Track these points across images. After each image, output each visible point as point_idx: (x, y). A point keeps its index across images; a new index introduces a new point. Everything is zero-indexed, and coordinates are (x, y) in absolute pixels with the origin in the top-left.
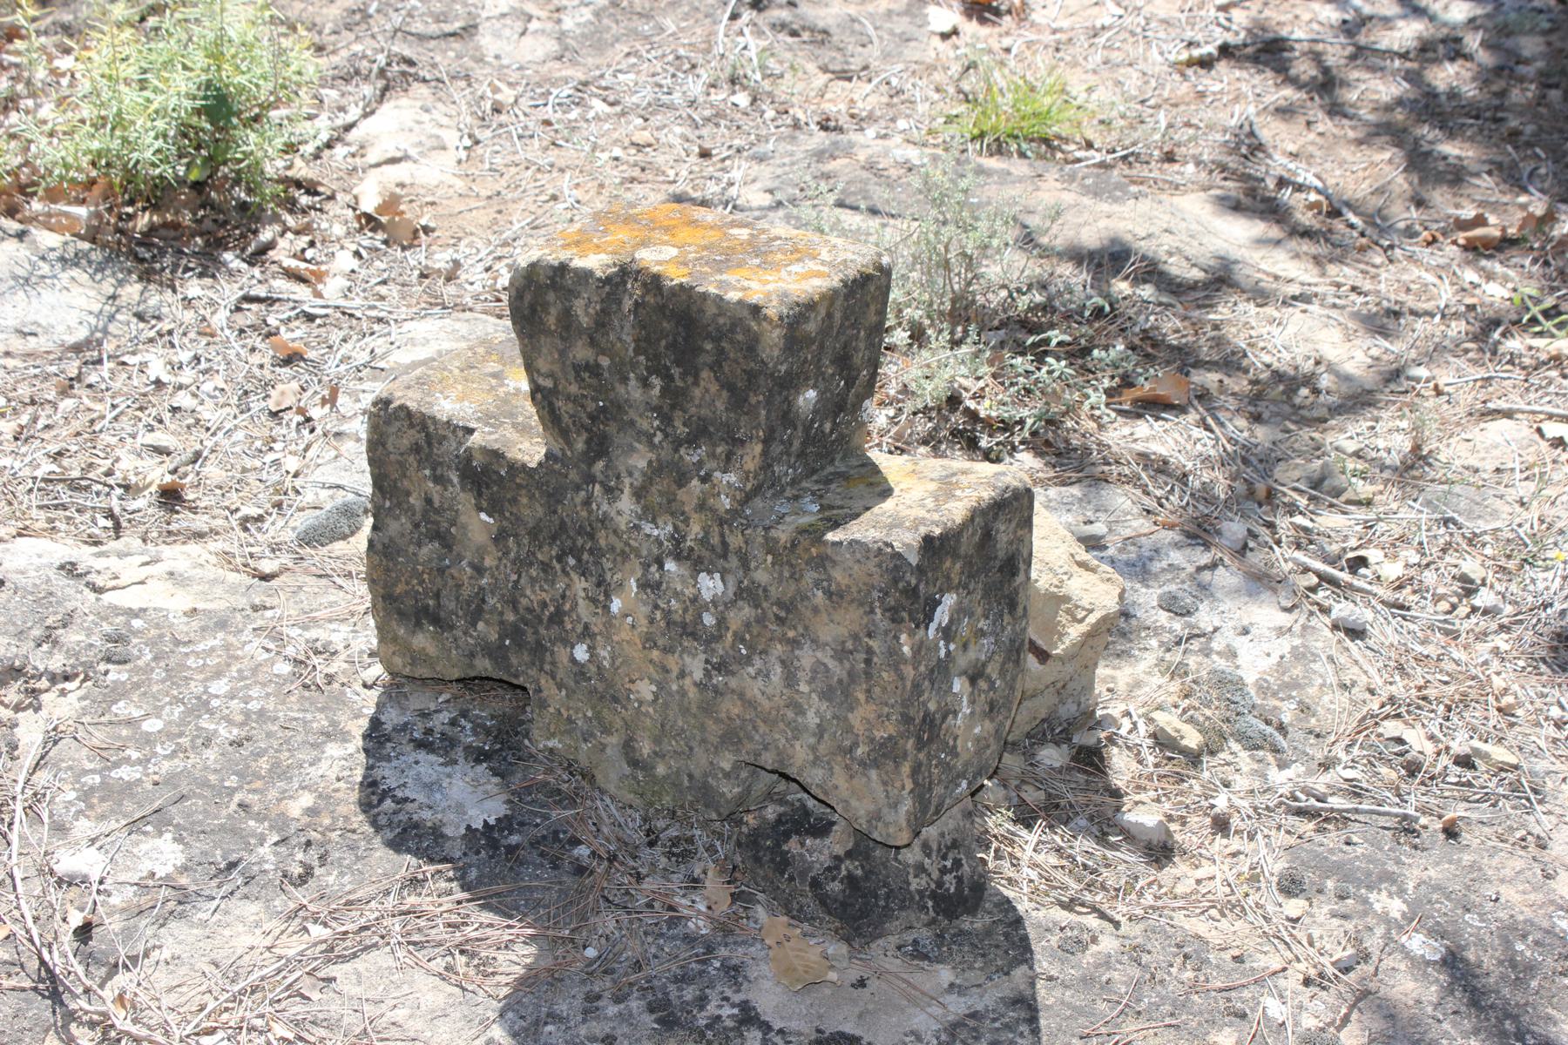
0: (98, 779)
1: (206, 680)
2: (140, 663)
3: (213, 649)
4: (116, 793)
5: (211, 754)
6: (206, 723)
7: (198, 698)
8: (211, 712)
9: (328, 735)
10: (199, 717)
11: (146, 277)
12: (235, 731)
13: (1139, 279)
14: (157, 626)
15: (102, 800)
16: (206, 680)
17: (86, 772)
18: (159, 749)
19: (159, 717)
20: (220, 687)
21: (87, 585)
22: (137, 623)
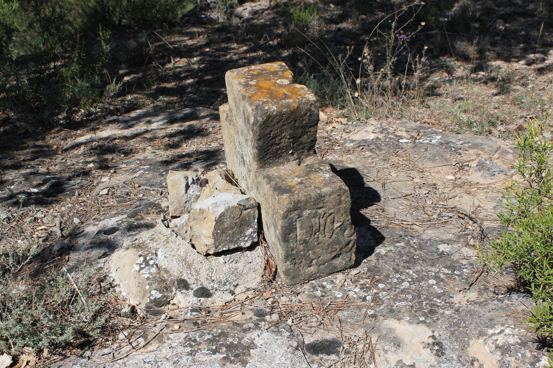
0: (455, 272)
1: (409, 289)
2: (428, 302)
3: (400, 301)
4: (452, 268)
5: (418, 268)
6: (415, 276)
7: (414, 283)
8: (412, 278)
9: (382, 257)
10: (417, 278)
11: (352, 224)
12: (407, 271)
13: (245, 63)
14: (415, 316)
15: (456, 267)
16: (409, 289)
17: (459, 276)
18: (433, 274)
19: (429, 284)
20: (406, 284)
21: (436, 339)
22: (422, 319)
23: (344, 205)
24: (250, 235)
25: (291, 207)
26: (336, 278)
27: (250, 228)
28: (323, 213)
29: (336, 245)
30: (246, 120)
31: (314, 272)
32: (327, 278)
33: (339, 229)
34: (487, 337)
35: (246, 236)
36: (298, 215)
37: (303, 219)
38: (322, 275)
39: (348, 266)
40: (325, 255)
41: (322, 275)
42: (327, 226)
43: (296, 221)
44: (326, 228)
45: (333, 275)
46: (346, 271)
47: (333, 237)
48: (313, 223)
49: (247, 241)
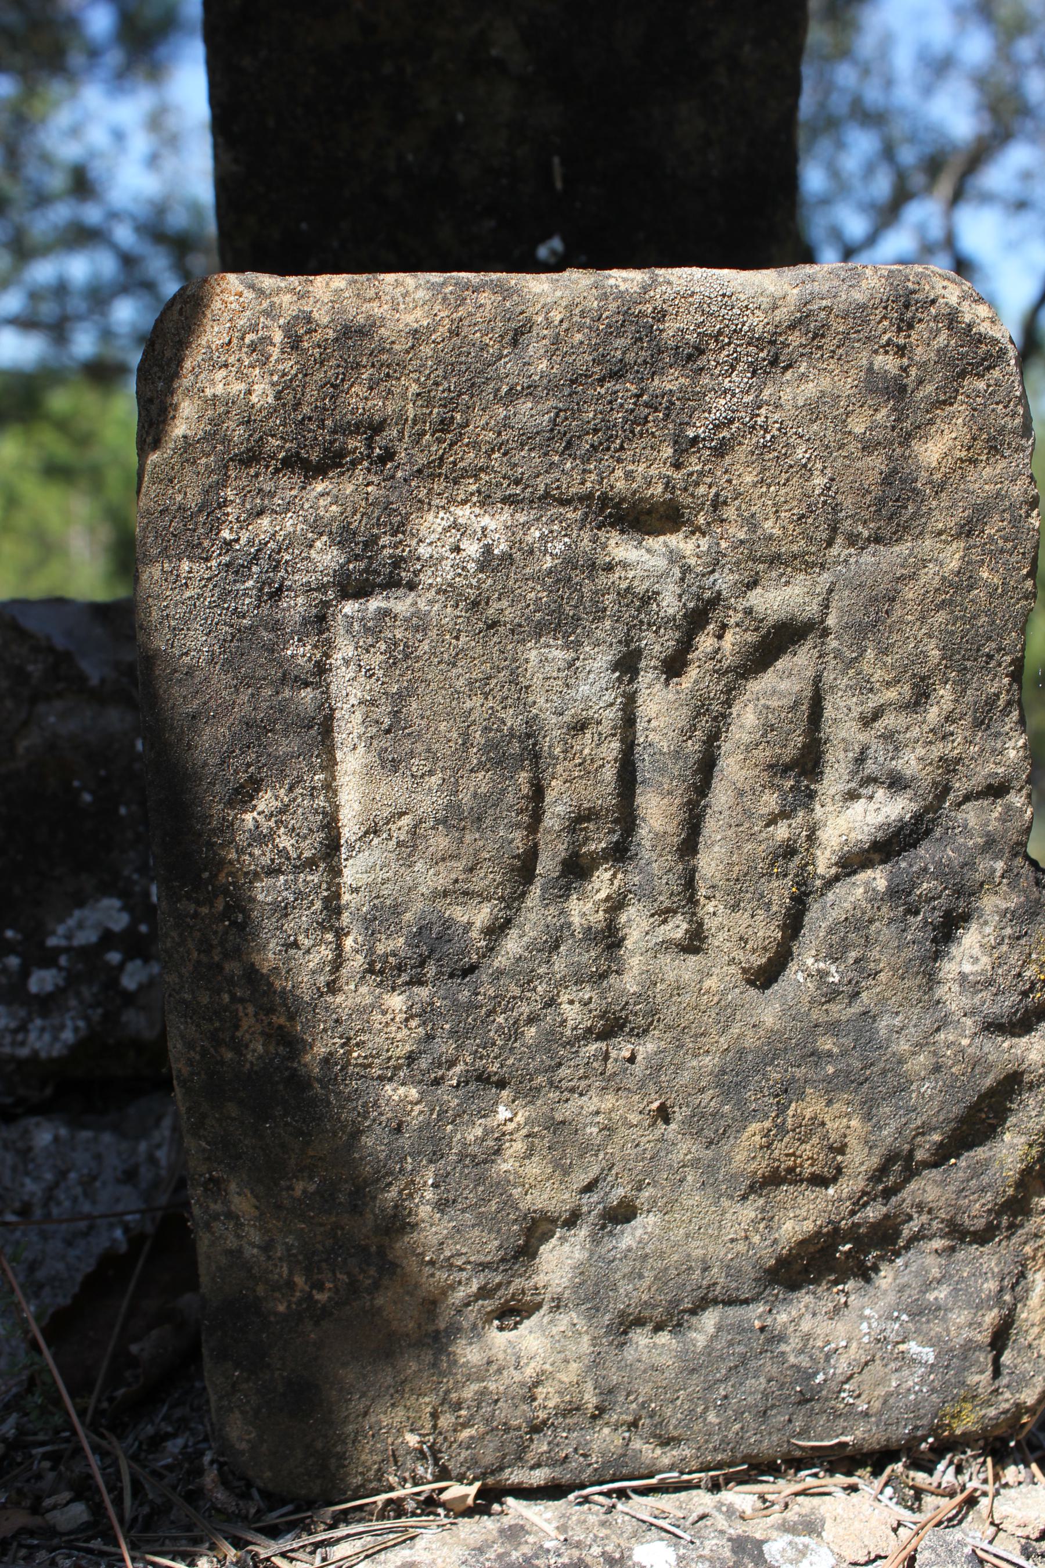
23: (952, 558)
24: (90, 955)
25: (262, 394)
26: (811, 1527)
27: (106, 889)
28: (670, 604)
29: (831, 1089)
30: (704, 722)
31: (549, 1397)
32: (702, 1500)
33: (878, 878)
34: (694, 1555)
35: (48, 959)
36: (344, 536)
37: (419, 624)
38: (648, 1452)
39: (968, 1422)
40: (693, 1198)
41: (648, 1452)
42: (721, 797)
43: (320, 621)
44: (713, 828)
45: (782, 1488)
46: (944, 1474)
47: (794, 975)
48: (541, 702)
49: (45, 1004)
